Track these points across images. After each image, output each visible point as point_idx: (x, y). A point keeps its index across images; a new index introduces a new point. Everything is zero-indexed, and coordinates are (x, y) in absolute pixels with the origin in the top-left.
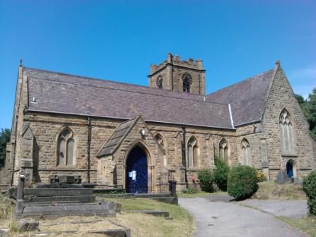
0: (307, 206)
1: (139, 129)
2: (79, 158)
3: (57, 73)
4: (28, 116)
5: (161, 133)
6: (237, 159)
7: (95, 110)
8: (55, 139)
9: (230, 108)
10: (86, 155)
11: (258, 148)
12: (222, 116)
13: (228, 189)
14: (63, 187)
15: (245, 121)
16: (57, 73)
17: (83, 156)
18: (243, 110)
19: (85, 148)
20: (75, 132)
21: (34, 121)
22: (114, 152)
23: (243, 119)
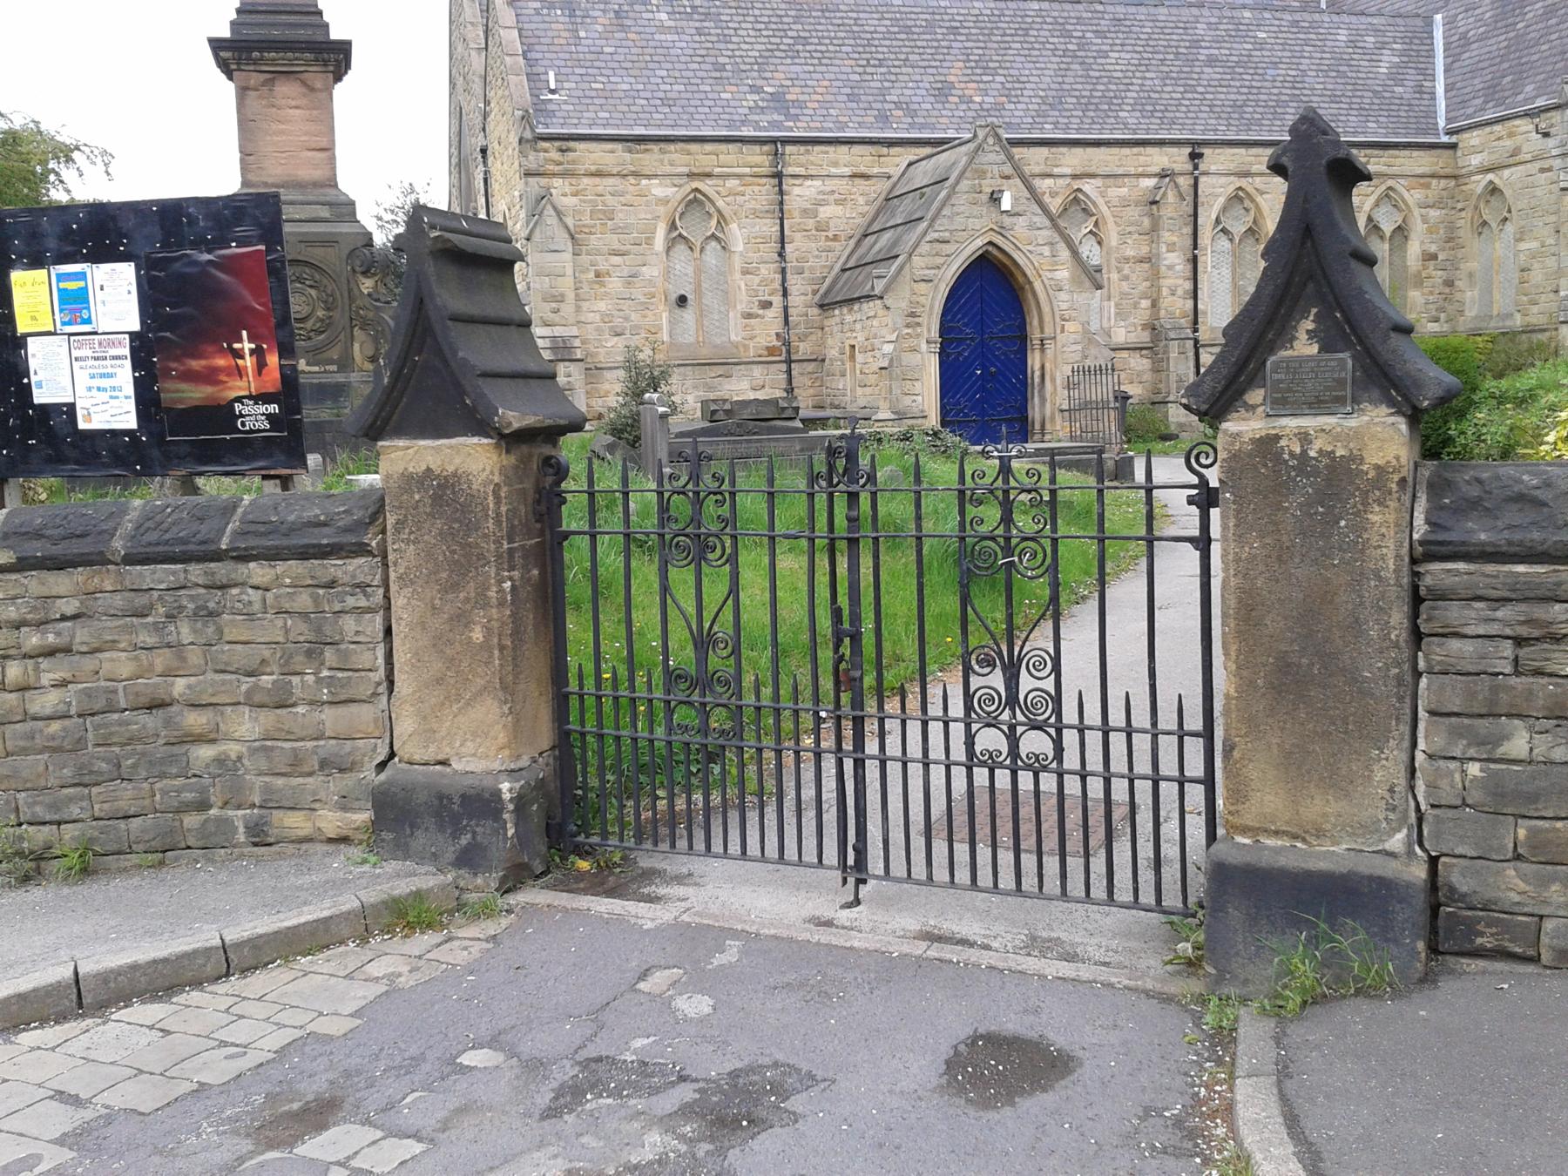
0: (1447, 986)
1: (988, 186)
2: (749, 316)
3: (1465, 636)
4: (534, 162)
5: (1088, 187)
6: (1449, 283)
7: (801, 105)
8: (650, 241)
9: (1438, 34)
10: (777, 300)
11: (1549, 230)
12: (1396, 77)
13: (1327, 356)
14: (749, 433)
15: (1500, 103)
16: (1465, 636)
17: (767, 305)
18: (1500, 42)
19: (769, 271)
20: (727, 211)
21: (563, 175)
22: (887, 289)
23: (1492, 92)
